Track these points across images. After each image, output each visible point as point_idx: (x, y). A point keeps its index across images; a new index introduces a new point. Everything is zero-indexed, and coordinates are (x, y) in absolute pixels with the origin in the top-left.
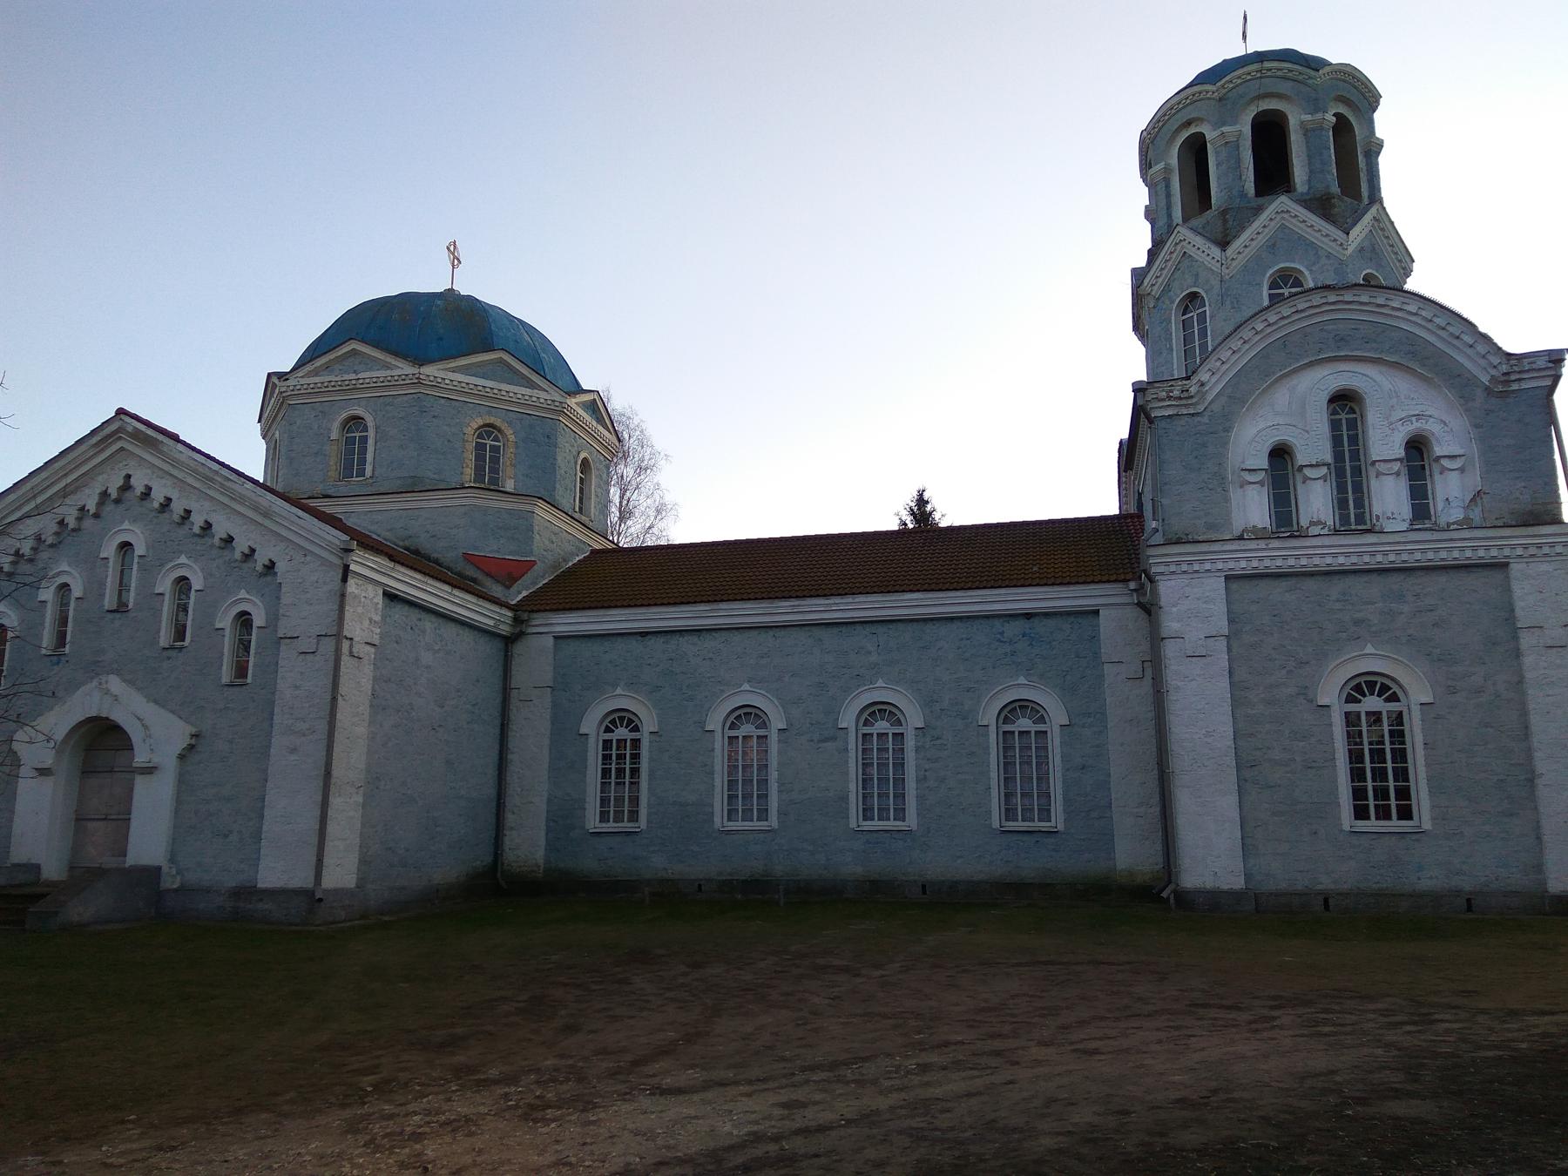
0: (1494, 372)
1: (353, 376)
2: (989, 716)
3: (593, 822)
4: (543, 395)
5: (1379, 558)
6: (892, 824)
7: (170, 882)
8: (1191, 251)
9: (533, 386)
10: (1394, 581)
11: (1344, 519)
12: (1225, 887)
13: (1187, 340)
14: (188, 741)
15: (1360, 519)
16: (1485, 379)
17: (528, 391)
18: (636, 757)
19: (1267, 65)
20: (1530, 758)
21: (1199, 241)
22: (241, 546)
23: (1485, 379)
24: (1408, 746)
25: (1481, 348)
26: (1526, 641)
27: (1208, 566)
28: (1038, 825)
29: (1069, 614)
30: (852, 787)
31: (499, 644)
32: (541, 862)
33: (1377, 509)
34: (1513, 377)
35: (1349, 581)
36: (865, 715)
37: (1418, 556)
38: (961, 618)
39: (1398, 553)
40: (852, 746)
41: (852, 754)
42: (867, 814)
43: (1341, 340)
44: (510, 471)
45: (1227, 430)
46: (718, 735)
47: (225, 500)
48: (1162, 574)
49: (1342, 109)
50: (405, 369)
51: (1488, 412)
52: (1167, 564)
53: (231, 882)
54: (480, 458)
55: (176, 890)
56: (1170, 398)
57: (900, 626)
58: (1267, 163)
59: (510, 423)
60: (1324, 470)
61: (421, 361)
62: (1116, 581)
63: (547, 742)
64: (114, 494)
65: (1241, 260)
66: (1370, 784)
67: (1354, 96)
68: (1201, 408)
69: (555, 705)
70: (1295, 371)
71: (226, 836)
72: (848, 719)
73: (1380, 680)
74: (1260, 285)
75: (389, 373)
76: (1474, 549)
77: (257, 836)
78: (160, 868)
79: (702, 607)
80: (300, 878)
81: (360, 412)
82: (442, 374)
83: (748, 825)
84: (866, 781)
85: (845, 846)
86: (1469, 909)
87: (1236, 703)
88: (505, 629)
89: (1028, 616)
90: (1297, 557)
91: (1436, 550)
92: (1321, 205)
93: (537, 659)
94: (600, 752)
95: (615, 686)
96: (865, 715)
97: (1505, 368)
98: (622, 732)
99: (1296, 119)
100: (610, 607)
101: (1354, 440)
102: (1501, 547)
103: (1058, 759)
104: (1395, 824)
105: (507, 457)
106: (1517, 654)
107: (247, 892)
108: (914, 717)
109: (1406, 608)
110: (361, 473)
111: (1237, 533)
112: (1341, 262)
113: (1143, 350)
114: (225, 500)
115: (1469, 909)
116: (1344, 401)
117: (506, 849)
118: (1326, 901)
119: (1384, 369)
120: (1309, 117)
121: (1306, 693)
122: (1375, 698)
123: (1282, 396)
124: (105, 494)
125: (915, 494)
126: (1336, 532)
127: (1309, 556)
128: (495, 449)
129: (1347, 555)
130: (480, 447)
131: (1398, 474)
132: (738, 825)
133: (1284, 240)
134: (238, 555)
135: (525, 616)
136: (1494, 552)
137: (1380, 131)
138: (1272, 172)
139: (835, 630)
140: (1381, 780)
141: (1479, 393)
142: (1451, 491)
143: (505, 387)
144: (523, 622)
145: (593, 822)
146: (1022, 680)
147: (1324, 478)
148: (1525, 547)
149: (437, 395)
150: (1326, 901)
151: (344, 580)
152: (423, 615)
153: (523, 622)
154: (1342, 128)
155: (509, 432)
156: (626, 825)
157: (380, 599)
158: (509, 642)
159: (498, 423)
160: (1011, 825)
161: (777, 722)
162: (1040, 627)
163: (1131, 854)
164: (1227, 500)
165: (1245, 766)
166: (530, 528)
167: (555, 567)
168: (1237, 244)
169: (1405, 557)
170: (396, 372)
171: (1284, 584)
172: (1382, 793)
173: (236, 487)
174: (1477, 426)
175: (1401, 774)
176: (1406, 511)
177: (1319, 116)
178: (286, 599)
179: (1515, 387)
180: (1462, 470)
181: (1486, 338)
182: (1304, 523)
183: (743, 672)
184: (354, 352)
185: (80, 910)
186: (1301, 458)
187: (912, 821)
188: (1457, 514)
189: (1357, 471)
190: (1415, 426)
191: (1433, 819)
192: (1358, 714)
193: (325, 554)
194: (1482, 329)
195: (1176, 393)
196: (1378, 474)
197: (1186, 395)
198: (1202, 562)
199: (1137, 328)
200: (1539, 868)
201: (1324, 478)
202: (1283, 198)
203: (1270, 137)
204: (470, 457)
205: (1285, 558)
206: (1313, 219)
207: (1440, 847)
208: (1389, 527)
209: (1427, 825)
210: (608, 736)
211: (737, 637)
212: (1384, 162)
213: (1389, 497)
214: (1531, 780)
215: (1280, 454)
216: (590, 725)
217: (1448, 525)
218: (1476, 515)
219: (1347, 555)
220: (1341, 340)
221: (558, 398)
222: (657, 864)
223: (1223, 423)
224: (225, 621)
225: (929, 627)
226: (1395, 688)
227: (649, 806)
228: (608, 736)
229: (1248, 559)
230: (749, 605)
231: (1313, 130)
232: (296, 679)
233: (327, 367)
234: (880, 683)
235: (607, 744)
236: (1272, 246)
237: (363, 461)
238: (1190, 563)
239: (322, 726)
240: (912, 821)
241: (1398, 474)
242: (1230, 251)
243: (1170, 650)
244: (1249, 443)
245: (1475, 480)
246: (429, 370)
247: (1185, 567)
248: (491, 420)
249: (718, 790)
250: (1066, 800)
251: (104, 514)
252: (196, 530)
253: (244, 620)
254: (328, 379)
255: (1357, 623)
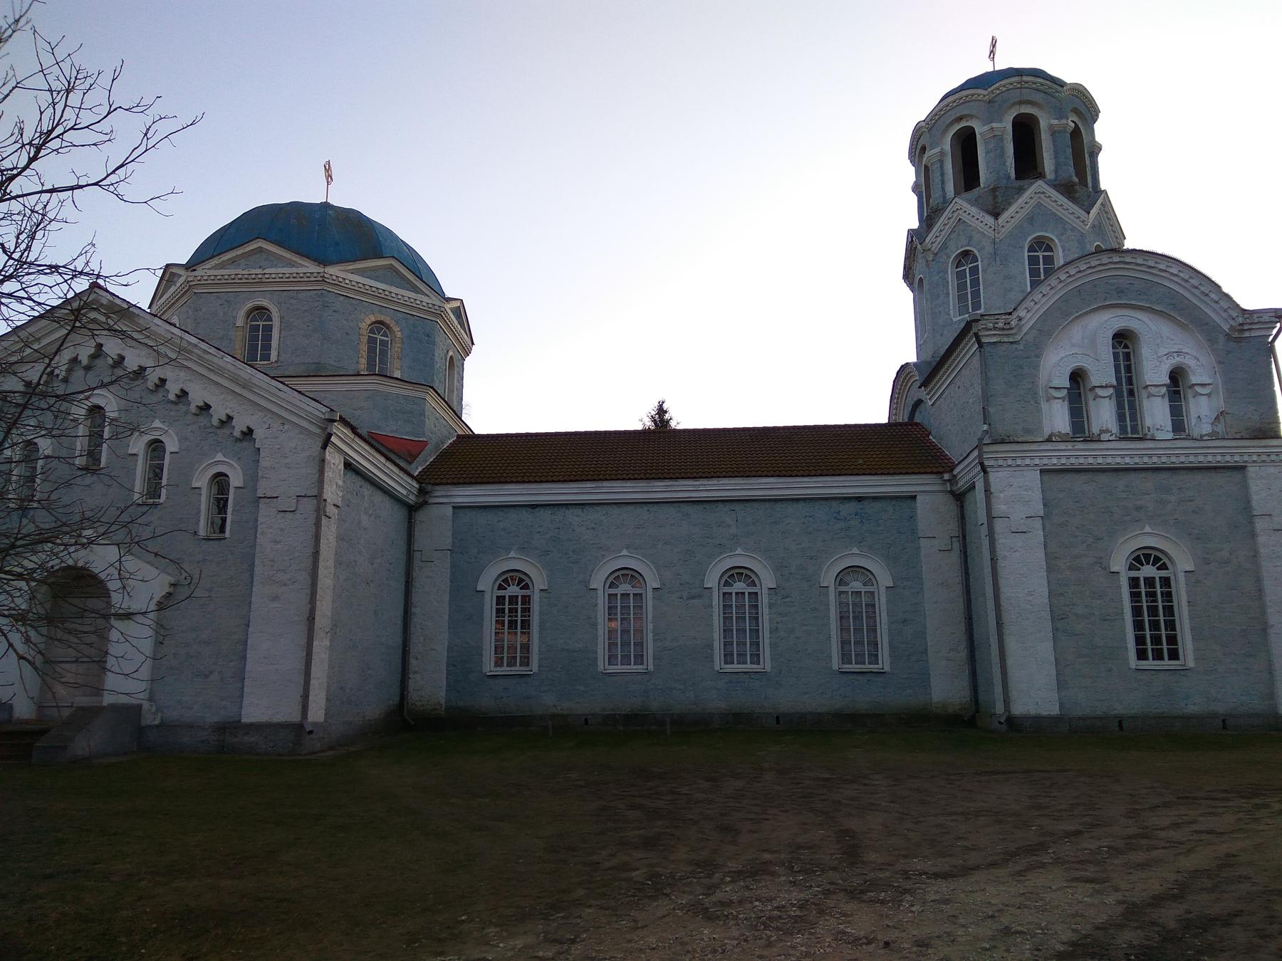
0: (1232, 323)
1: (259, 271)
2: (828, 579)
3: (489, 667)
4: (426, 299)
5: (1155, 459)
6: (749, 667)
7: (150, 718)
8: (965, 217)
9: (415, 289)
10: (1163, 476)
11: (1123, 429)
12: (1045, 713)
13: (961, 287)
14: (167, 589)
15: (1134, 430)
16: (1226, 328)
17: (413, 295)
18: (527, 611)
19: (1025, 78)
20: (1264, 613)
21: (973, 210)
22: (218, 413)
23: (1226, 328)
24: (1175, 604)
25: (1224, 304)
26: (1260, 525)
27: (1027, 461)
28: (868, 667)
29: (892, 498)
30: (716, 636)
31: (399, 515)
32: (443, 702)
33: (1148, 422)
34: (1246, 327)
35: (1132, 476)
36: (726, 577)
37: (1183, 459)
38: (804, 499)
39: (1169, 456)
40: (715, 602)
41: (716, 609)
42: (728, 658)
43: (1120, 291)
44: (397, 363)
45: (1038, 356)
46: (600, 593)
47: (205, 372)
48: (992, 466)
49: (1076, 119)
50: (312, 268)
51: (1228, 352)
52: (996, 459)
53: (212, 718)
54: (371, 350)
55: (157, 726)
56: (995, 328)
57: (755, 505)
58: (1008, 155)
59: (397, 322)
60: (1111, 391)
61: (324, 262)
62: (931, 473)
63: (446, 597)
64: (85, 360)
65: (1009, 227)
66: (1148, 633)
67: (1082, 109)
68: (1018, 338)
69: (453, 566)
70: (1086, 313)
71: (207, 676)
72: (712, 580)
73: (1154, 553)
74: (1022, 248)
75: (294, 270)
76: (1223, 455)
77: (240, 676)
78: (140, 706)
79: (589, 485)
80: (287, 712)
81: (265, 303)
82: (342, 275)
83: (625, 668)
84: (727, 631)
85: (712, 683)
86: (1225, 728)
87: (1050, 569)
88: (412, 499)
89: (860, 499)
90: (1095, 457)
91: (1196, 455)
92: (1068, 190)
93: (438, 523)
94: (494, 607)
95: (508, 550)
96: (726, 577)
97: (1240, 320)
98: (513, 590)
99: (1045, 122)
100: (506, 482)
101: (1128, 368)
102: (1241, 454)
103: (884, 614)
104: (1166, 663)
105: (395, 350)
106: (1253, 535)
107: (231, 727)
108: (767, 579)
109: (1172, 498)
110: (266, 357)
111: (1046, 437)
112: (1082, 235)
113: (911, 294)
114: (205, 372)
115: (1225, 728)
116: (1123, 339)
117: (411, 689)
118: (1120, 722)
119: (1151, 316)
120: (1056, 122)
121: (1102, 563)
122: (1150, 566)
123: (1077, 332)
124: (75, 361)
125: (656, 404)
126: (1121, 439)
127: (1104, 456)
128: (383, 343)
129: (1131, 456)
130: (371, 341)
131: (1163, 396)
132: (618, 668)
133: (1037, 216)
134: (215, 422)
135: (429, 488)
136: (1237, 458)
137: (1099, 137)
138: (1027, 163)
139: (700, 507)
140: (1156, 632)
141: (1222, 339)
142: (1201, 410)
143: (394, 290)
144: (427, 493)
145: (489, 667)
146: (855, 550)
147: (1110, 397)
148: (1259, 455)
149: (329, 290)
150: (1120, 722)
151: (324, 447)
152: (367, 485)
153: (427, 493)
154: (1076, 134)
155: (396, 329)
156: (518, 669)
157: (342, 466)
158: (412, 510)
159: (387, 320)
160: (847, 667)
161: (652, 582)
162: (869, 508)
163: (946, 688)
164: (1039, 410)
165: (1057, 618)
166: (422, 414)
167: (437, 446)
168: (1004, 217)
169: (1173, 459)
170: (301, 270)
171: (1083, 477)
172: (1156, 640)
173: (216, 360)
174: (1219, 363)
175: (1171, 625)
176: (1169, 425)
177: (1064, 121)
178: (265, 463)
179: (1247, 334)
180: (1209, 395)
181: (1227, 296)
182: (1095, 430)
183: (623, 539)
184: (260, 250)
185: (82, 745)
186: (1094, 380)
187: (767, 664)
188: (1206, 429)
189: (1131, 393)
190: (1176, 360)
191: (1196, 659)
192: (1138, 579)
193: (305, 424)
194: (1225, 290)
195: (1001, 325)
196: (1150, 396)
197: (1007, 327)
198: (1023, 458)
199: (908, 276)
200: (1271, 695)
201: (1110, 397)
202: (1040, 182)
203: (1025, 132)
204: (364, 348)
205: (1086, 457)
206: (1063, 200)
207: (1202, 680)
208: (1159, 436)
209: (1191, 664)
210: (501, 593)
211: (616, 511)
212: (1102, 159)
213: (1156, 413)
214: (1265, 630)
215: (1077, 377)
216: (486, 583)
217: (1202, 436)
218: (1220, 428)
219: (1131, 456)
220: (1120, 291)
221: (438, 303)
222: (549, 702)
223: (1035, 351)
224: (202, 481)
225: (779, 506)
226: (1165, 560)
227: (540, 652)
228: (501, 593)
229: (1059, 457)
230: (629, 484)
231: (1060, 132)
232: (276, 536)
233: (233, 261)
234: (739, 551)
235: (500, 600)
236: (1031, 219)
237: (267, 347)
238: (1014, 459)
239: (304, 578)
240: (767, 664)
241: (1163, 396)
242: (1000, 220)
243: (999, 526)
244: (1055, 365)
245: (1219, 403)
246: (332, 270)
247: (1010, 462)
248: (382, 318)
249: (600, 639)
250: (892, 646)
251: (72, 379)
252: (172, 397)
253: (220, 480)
254: (233, 272)
255: (1138, 508)
